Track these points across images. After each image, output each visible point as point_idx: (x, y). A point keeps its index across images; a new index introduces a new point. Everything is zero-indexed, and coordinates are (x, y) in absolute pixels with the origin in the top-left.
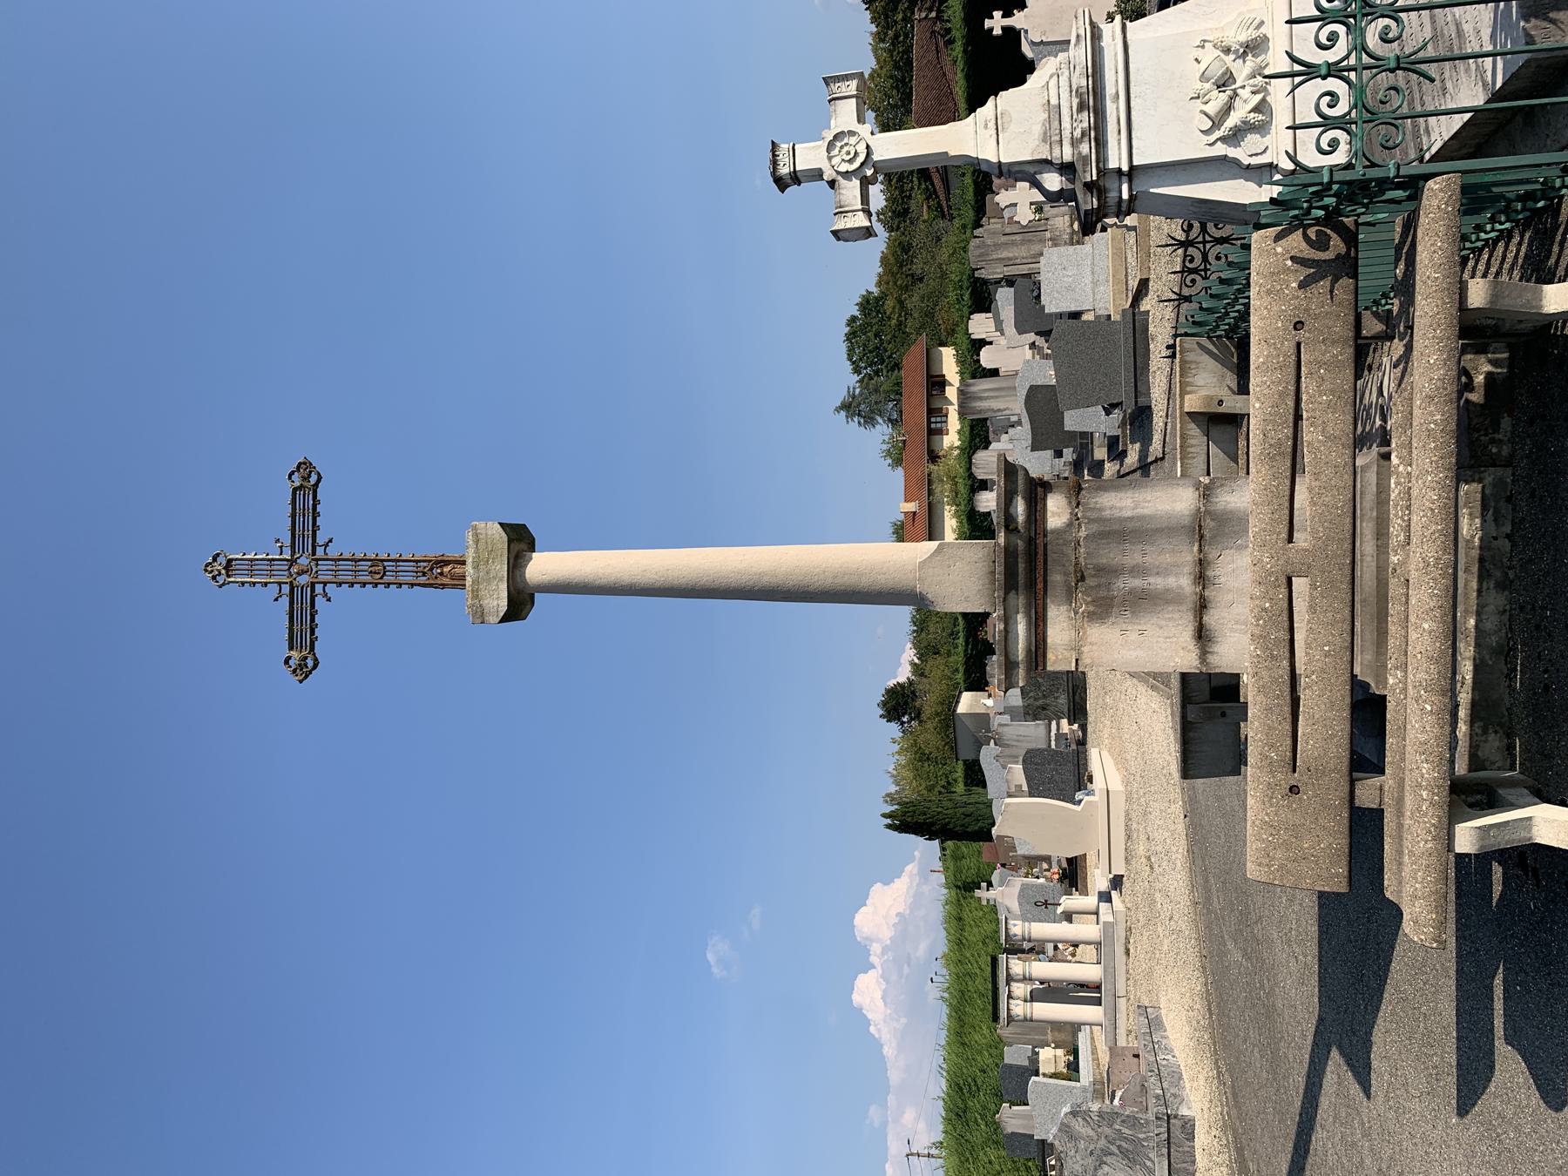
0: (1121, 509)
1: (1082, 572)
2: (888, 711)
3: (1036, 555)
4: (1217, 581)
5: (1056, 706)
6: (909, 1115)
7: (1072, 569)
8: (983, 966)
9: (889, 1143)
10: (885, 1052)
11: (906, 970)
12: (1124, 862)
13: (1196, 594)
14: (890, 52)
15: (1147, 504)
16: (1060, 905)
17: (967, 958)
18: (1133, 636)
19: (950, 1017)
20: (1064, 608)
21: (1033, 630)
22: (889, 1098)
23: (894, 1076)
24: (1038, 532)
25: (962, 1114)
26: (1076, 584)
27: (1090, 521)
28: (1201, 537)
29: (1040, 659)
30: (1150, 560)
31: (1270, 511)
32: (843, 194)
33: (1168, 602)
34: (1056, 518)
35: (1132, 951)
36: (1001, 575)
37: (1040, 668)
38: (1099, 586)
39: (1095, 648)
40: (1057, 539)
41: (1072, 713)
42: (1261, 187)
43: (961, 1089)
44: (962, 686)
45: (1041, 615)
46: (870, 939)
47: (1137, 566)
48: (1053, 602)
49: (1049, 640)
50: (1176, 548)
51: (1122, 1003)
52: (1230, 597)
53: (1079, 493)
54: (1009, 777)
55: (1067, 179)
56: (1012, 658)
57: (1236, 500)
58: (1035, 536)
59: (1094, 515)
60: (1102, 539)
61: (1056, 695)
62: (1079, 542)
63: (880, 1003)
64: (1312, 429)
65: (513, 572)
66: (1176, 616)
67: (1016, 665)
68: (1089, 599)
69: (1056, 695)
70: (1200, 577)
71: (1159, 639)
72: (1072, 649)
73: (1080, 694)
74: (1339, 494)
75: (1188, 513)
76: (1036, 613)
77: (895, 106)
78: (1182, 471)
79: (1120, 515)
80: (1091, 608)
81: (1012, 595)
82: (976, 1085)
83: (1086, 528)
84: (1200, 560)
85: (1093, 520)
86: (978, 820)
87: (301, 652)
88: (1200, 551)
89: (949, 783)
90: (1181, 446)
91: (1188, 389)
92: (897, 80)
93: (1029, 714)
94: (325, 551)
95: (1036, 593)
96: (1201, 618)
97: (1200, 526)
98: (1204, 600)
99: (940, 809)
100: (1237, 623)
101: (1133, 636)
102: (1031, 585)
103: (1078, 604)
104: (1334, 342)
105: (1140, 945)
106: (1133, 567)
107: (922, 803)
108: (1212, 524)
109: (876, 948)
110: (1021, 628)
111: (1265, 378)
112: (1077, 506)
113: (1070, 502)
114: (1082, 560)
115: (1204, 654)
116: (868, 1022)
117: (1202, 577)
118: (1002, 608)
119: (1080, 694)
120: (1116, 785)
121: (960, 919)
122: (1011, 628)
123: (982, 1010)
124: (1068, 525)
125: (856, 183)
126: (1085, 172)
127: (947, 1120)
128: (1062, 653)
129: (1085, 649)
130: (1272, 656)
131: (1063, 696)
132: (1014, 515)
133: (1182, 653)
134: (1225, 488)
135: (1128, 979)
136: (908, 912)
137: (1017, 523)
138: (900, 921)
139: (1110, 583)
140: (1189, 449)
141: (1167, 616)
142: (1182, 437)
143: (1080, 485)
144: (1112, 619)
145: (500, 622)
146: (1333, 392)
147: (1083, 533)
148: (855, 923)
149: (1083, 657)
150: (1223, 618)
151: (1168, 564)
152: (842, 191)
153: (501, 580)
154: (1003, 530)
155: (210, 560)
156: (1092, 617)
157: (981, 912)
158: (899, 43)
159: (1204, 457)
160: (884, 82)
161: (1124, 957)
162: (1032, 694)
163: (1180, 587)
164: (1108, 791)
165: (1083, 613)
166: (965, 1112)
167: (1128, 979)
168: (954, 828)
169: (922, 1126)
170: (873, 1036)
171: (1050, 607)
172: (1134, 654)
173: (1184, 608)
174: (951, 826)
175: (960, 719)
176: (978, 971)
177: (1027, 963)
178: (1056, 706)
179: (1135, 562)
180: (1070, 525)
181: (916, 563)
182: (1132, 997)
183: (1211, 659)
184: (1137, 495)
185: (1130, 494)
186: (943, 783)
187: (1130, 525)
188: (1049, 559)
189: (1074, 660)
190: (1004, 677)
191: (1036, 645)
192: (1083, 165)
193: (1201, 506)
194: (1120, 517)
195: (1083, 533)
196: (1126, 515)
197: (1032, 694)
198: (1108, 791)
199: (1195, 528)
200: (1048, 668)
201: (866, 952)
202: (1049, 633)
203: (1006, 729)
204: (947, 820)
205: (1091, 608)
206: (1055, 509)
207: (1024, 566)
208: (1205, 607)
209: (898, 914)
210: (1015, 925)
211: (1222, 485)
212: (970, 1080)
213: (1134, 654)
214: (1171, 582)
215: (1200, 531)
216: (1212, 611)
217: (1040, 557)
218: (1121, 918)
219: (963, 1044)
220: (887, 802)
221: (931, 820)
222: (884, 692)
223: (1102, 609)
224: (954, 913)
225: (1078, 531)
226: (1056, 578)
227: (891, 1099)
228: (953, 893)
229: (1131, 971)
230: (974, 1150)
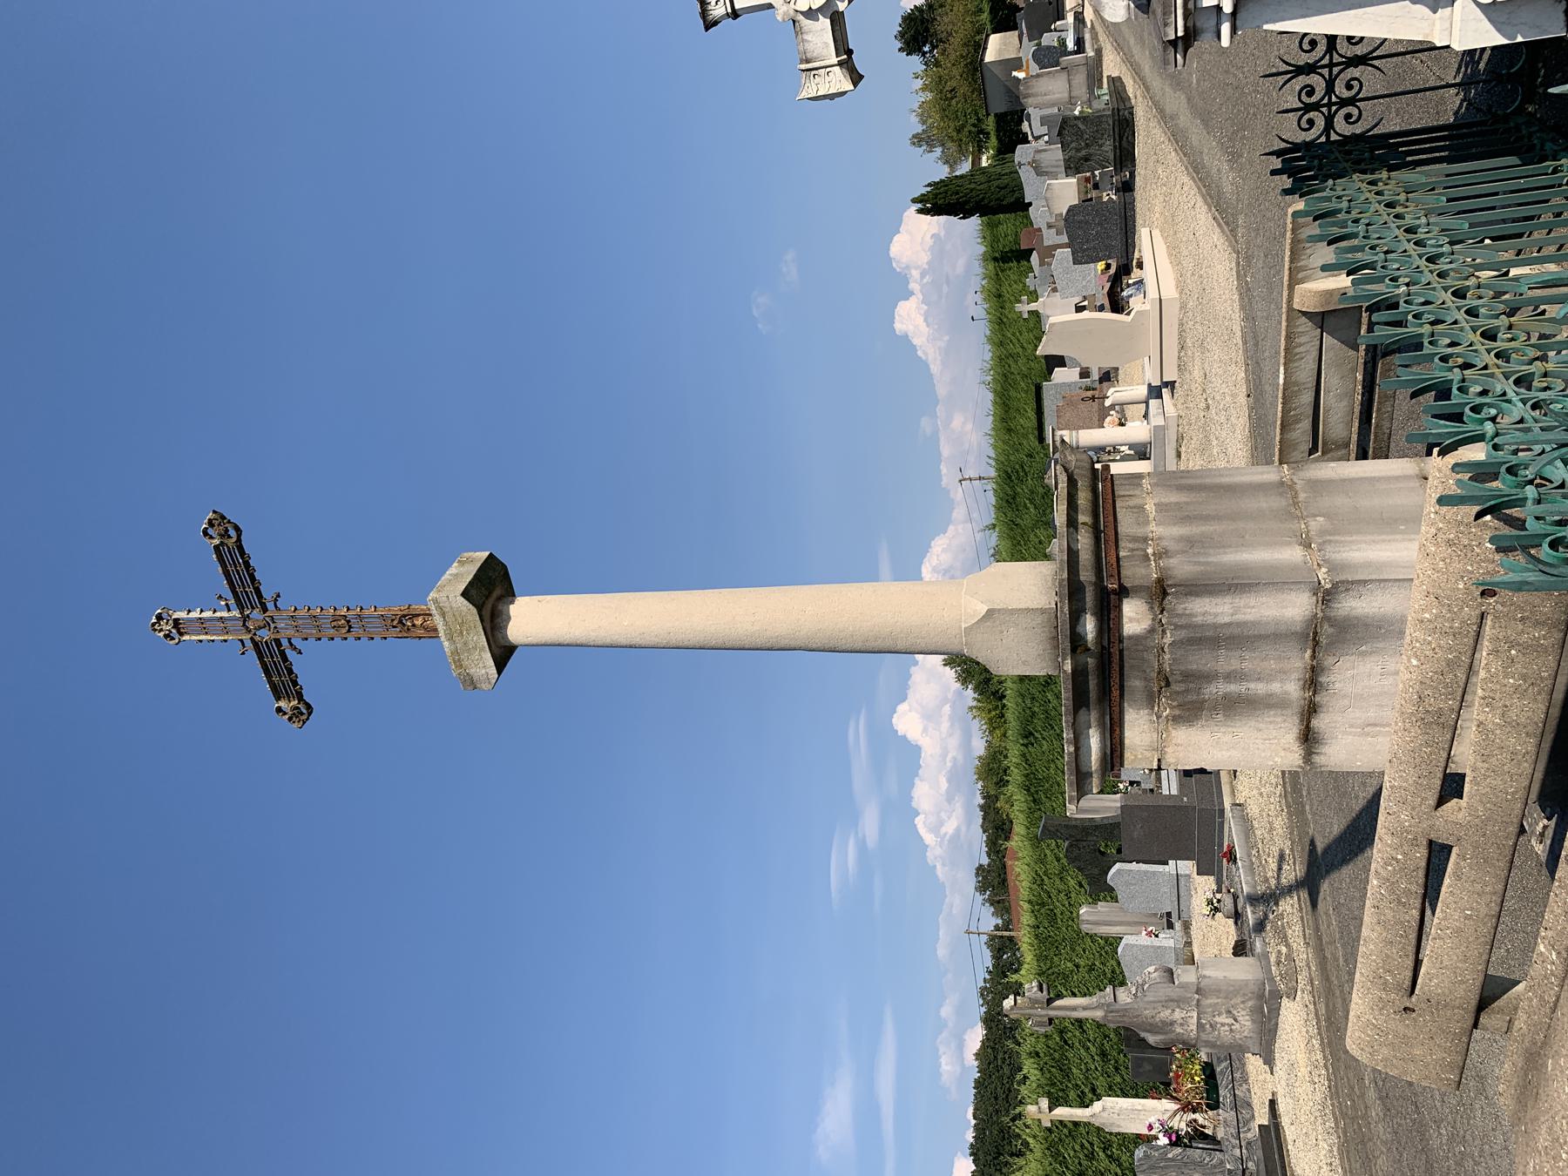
0: (1216, 615)
2: (907, 43)
5: (1100, 155)
6: (957, 422)
9: (941, 447)
11: (945, 289)
12: (1177, 369)
15: (1249, 610)
19: (995, 403)
20: (1144, 712)
21: (1108, 735)
22: (937, 410)
23: (942, 391)
24: (1112, 640)
25: (1011, 501)
27: (1177, 627)
28: (1316, 643)
31: (1417, 775)
32: (808, 41)
33: (1270, 706)
36: (1067, 700)
37: (1116, 768)
40: (1137, 645)
41: (1118, 161)
42: (1435, 12)
43: (1010, 477)
44: (989, 27)
46: (908, 267)
47: (1235, 671)
48: (1130, 705)
49: (1127, 742)
52: (1346, 702)
53: (1163, 599)
54: (1048, 195)
55: (1136, 7)
56: (1084, 769)
58: (1109, 644)
59: (1183, 621)
61: (1100, 142)
62: (1163, 648)
63: (923, 326)
64: (1487, 709)
65: (493, 636)
66: (1279, 719)
67: (1090, 775)
69: (1100, 142)
71: (1257, 741)
72: (1154, 750)
73: (1127, 138)
74: (1511, 781)
75: (1301, 618)
76: (1111, 719)
78: (1285, 379)
80: (1177, 712)
81: (1083, 712)
82: (1024, 470)
86: (1015, 191)
87: (290, 701)
88: (1313, 657)
89: (979, 120)
90: (1286, 350)
93: (1070, 168)
94: (276, 606)
95: (1111, 700)
96: (1309, 722)
97: (1315, 633)
99: (972, 186)
100: (1351, 726)
102: (1105, 692)
103: (1162, 708)
104: (1537, 623)
107: (954, 182)
108: (1331, 630)
109: (915, 274)
110: (1094, 741)
111: (1430, 638)
112: (1162, 612)
113: (1152, 608)
115: (1308, 755)
116: (914, 348)
117: (1313, 681)
118: (1071, 732)
119: (1127, 138)
120: (1170, 292)
121: (999, 296)
122: (1083, 750)
123: (1026, 392)
124: (1149, 632)
125: (825, 23)
126: (1166, 25)
127: (998, 508)
128: (1142, 753)
130: (1399, 902)
131: (1108, 143)
132: (1083, 634)
136: (942, 234)
137: (1086, 641)
138: (934, 242)
140: (1297, 350)
142: (1288, 337)
143: (1165, 590)
145: (499, 672)
146: (1524, 677)
147: (1168, 639)
148: (892, 255)
150: (1335, 722)
152: (805, 37)
153: (482, 649)
154: (1069, 657)
155: (154, 620)
156: (1176, 720)
157: (1021, 285)
159: (1315, 354)
162: (1073, 145)
164: (1160, 300)
165: (1168, 716)
166: (1014, 498)
168: (989, 202)
169: (969, 426)
170: (920, 358)
171: (1128, 711)
172: (1226, 754)
173: (1289, 712)
174: (986, 201)
175: (988, 67)
178: (1100, 155)
180: (1152, 631)
181: (960, 627)
183: (1318, 759)
184: (1237, 600)
185: (1228, 599)
186: (973, 121)
188: (1126, 664)
189: (1156, 760)
191: (1112, 749)
192: (1164, 14)
194: (1214, 624)
195: (1168, 639)
196: (1223, 622)
197: (1073, 145)
198: (1160, 300)
201: (904, 279)
202: (1126, 735)
203: (1043, 156)
204: (981, 196)
205: (1177, 712)
206: (1132, 615)
207: (1095, 682)
208: (1315, 712)
209: (933, 236)
211: (1347, 590)
212: (1017, 467)
213: (1226, 754)
214: (1276, 687)
216: (1322, 715)
217: (1116, 667)
219: (1009, 430)
220: (914, 144)
221: (964, 199)
222: (900, 21)
223: (1191, 711)
224: (994, 290)
225: (1162, 638)
226: (1134, 683)
227: (940, 410)
228: (991, 267)
230: (1025, 533)
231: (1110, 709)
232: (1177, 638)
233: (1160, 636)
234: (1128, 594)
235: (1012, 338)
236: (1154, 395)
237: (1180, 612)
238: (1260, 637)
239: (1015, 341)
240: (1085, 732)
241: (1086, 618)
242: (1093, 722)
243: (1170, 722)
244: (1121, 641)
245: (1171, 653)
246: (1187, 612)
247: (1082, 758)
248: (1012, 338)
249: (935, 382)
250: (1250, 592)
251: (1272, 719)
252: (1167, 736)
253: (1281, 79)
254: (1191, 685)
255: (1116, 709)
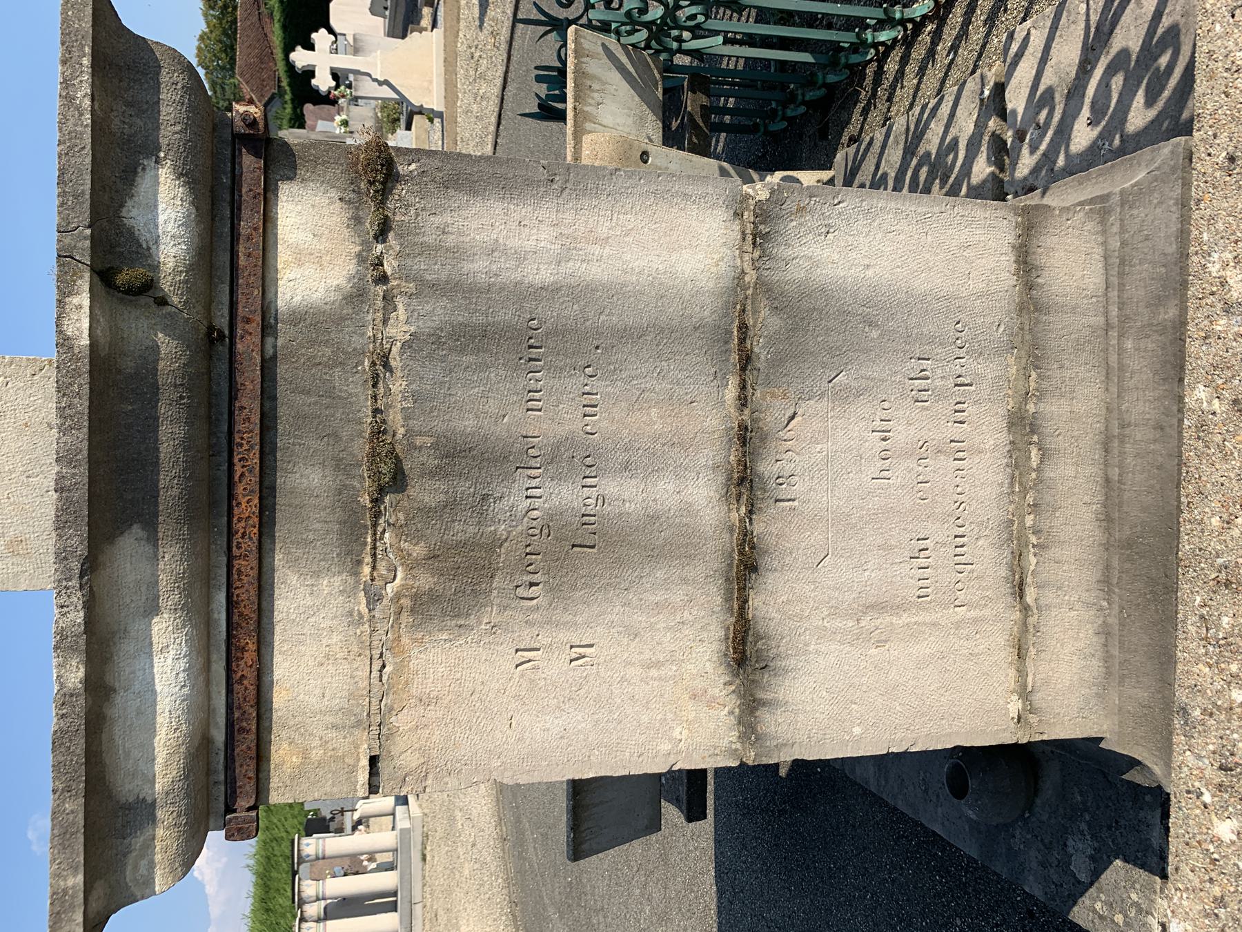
0: (521, 257)
1: (398, 462)
3: (232, 398)
4: (784, 491)
7: (361, 448)
8: (289, 829)
10: (207, 891)
13: (731, 529)
14: (220, 19)
15: (596, 250)
16: (356, 810)
17: (275, 824)
18: (554, 666)
19: (256, 884)
20: (331, 584)
23: (215, 911)
24: (242, 311)
26: (376, 501)
27: (426, 288)
28: (746, 361)
29: (245, 769)
30: (605, 424)
33: (657, 553)
34: (309, 270)
35: (428, 858)
37: (243, 803)
38: (450, 506)
39: (433, 713)
40: (313, 343)
45: (249, 610)
48: (294, 563)
49: (280, 699)
50: (680, 391)
51: (418, 909)
56: (126, 789)
57: (836, 256)
59: (435, 271)
60: (462, 351)
67: (143, 811)
68: (418, 550)
70: (742, 481)
72: (358, 724)
75: (711, 284)
76: (231, 604)
77: (223, 68)
79: (518, 276)
80: (425, 581)
81: (129, 545)
83: (411, 312)
84: (743, 428)
85: (433, 286)
88: (743, 401)
91: (588, 126)
92: (226, 46)
95: (230, 533)
96: (744, 602)
97: (743, 327)
98: (753, 548)
101: (554, 666)
103: (382, 567)
105: (438, 856)
112: (382, 234)
113: (357, 220)
114: (395, 419)
118: (77, 599)
122: (123, 705)
129: (402, 721)
133: (690, 710)
134: (810, 221)
135: (424, 885)
137: (156, 267)
139: (485, 498)
144: (491, 614)
147: (399, 328)
149: (395, 750)
158: (228, 13)
160: (213, 45)
161: (421, 864)
163: (688, 509)
165: (398, 596)
167: (424, 885)
170: (196, 878)
176: (284, 834)
177: (321, 882)
179: (562, 430)
180: (356, 297)
182: (428, 904)
183: (773, 723)
184: (569, 217)
185: (547, 212)
187: (548, 313)
188: (282, 411)
189: (365, 762)
190: (80, 878)
193: (748, 268)
195: (399, 328)
199: (730, 332)
200: (275, 798)
202: (278, 673)
205: (425, 581)
210: (308, 845)
211: (801, 209)
215: (742, 341)
217: (249, 404)
218: (418, 824)
219: (268, 910)
225: (385, 321)
229: (427, 879)
231: (229, 567)
232: (427, 325)
233: (380, 315)
234: (294, 167)
235: (278, 823)
236: (401, 802)
237: (430, 239)
238: (627, 335)
239: (280, 827)
240: (136, 626)
241: (156, 182)
242: (169, 598)
244: (268, 327)
245: (409, 375)
246: (450, 240)
247: (120, 736)
248: (278, 823)
249: (210, 903)
250: (597, 192)
251: (659, 597)
253: (543, 29)
254: (465, 487)
255: (247, 566)
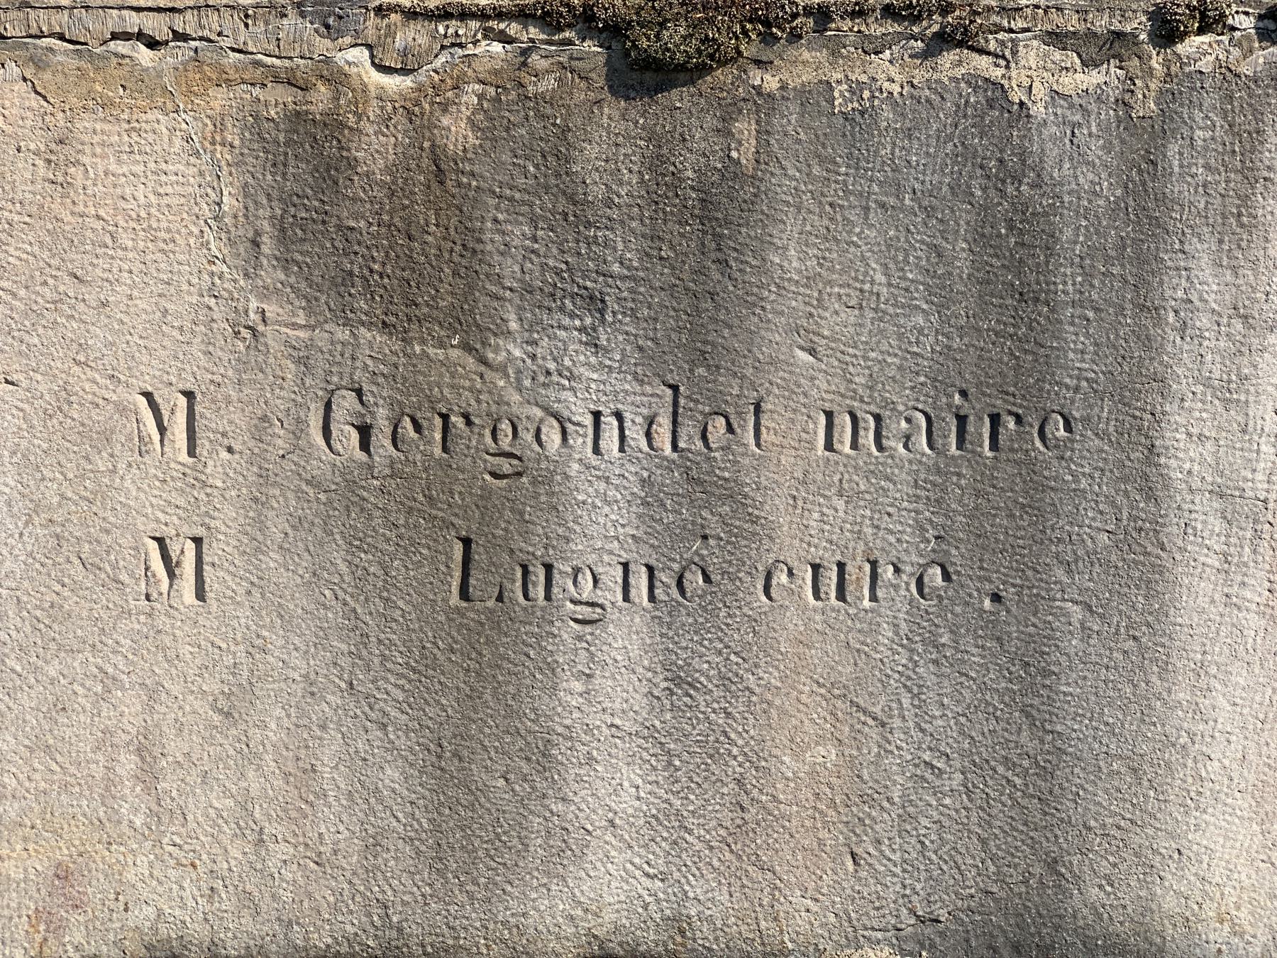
1: (688, 72)
30: (792, 621)
50: (885, 823)
60: (982, 238)
75: (1170, 903)
85: (1152, 163)
106: (733, 494)
139: (595, 303)
141: (327, 755)
151: (755, 760)
165: (337, 79)
225: (1056, 38)
243: (278, 98)
251: (332, 776)
252: (139, 82)
